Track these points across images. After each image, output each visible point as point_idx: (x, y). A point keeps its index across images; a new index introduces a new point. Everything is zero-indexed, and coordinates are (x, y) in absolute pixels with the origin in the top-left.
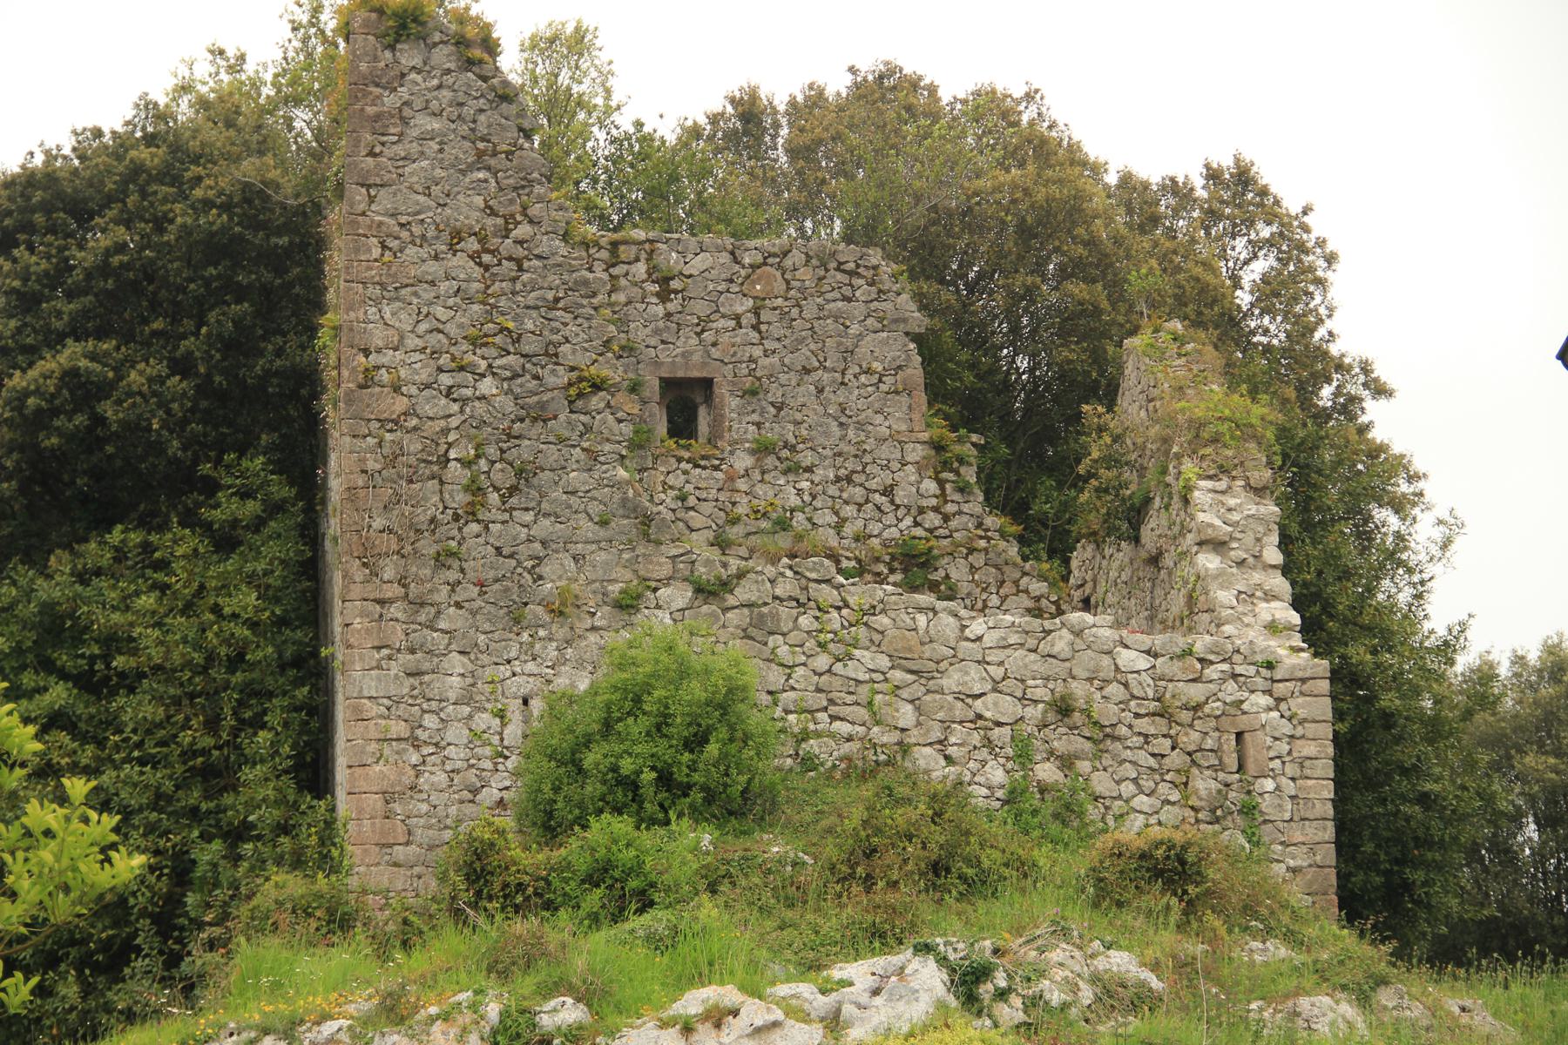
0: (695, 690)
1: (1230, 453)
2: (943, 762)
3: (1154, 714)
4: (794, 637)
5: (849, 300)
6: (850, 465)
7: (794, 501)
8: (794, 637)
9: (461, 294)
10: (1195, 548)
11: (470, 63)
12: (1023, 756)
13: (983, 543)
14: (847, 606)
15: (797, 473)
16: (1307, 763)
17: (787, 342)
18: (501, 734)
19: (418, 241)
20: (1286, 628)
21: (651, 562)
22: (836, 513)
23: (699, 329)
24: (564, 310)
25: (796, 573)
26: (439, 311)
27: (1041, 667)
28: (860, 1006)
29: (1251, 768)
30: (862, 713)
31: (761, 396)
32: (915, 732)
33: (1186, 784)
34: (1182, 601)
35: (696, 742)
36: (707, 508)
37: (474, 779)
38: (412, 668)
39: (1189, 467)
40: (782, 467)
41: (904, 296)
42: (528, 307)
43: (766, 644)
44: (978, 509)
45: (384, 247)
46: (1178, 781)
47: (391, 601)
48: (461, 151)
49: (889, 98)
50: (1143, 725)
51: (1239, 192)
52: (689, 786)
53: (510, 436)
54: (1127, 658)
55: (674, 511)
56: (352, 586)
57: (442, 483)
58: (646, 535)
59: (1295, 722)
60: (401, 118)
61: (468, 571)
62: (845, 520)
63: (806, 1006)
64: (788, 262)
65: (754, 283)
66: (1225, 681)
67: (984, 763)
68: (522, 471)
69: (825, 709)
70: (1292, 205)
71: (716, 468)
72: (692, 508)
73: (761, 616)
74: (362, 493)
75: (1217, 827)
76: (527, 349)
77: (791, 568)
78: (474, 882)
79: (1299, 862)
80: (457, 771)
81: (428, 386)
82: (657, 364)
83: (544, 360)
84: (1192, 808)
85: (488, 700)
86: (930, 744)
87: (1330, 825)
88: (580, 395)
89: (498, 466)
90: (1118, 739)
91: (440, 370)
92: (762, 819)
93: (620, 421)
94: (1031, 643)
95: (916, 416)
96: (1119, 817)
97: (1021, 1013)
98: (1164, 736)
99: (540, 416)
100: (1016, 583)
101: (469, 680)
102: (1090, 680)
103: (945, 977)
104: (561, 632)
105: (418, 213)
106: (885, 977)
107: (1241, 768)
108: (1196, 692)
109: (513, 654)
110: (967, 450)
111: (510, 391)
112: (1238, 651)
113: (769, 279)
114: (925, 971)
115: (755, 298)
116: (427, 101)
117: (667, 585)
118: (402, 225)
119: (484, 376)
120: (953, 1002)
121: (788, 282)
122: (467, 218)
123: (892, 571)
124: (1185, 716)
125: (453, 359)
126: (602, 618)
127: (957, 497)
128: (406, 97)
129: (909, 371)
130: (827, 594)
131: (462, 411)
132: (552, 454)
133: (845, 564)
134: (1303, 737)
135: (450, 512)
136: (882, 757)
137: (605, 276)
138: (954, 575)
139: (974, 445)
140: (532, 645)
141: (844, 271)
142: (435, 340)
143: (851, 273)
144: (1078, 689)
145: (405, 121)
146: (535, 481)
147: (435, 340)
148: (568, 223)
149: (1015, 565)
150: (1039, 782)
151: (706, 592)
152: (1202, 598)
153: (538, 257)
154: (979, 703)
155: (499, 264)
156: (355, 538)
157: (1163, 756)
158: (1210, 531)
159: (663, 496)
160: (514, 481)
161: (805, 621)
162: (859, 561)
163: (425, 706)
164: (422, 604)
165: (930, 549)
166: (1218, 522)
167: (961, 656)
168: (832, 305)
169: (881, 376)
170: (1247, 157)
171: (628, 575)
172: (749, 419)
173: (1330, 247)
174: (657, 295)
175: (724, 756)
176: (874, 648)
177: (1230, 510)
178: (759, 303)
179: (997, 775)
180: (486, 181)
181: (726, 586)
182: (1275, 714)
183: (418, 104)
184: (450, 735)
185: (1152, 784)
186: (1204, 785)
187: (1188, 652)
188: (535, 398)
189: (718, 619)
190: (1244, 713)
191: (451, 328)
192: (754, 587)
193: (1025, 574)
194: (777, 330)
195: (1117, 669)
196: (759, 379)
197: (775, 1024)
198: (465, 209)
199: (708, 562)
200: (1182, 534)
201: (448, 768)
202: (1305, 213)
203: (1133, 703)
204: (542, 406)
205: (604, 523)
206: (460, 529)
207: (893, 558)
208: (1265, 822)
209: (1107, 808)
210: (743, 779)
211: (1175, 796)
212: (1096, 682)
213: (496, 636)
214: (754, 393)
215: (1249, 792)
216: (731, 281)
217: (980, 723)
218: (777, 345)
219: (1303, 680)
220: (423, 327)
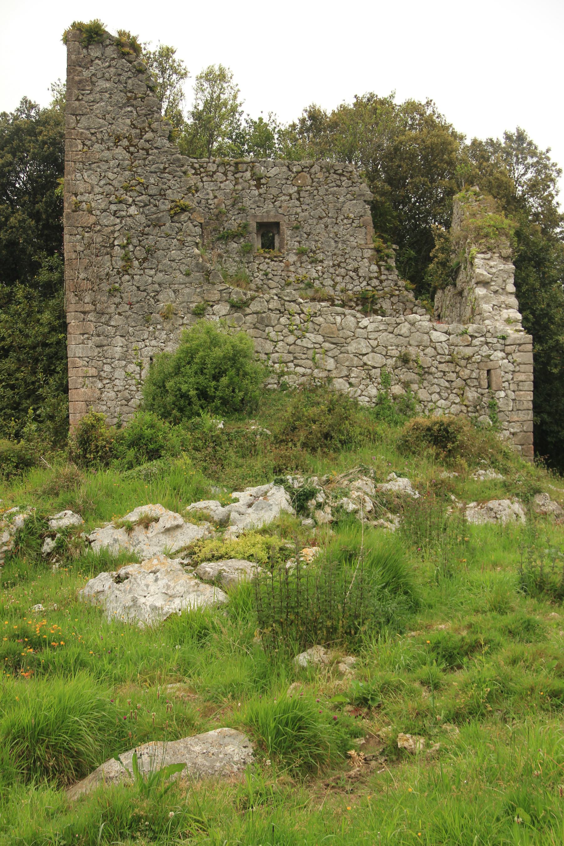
0: (218, 352)
1: (493, 241)
2: (348, 386)
3: (448, 362)
4: (278, 328)
5: (339, 186)
6: (339, 259)
7: (315, 275)
8: (278, 328)
9: (120, 166)
10: (475, 286)
11: (124, 55)
12: (386, 382)
13: (397, 292)
14: (303, 313)
15: (316, 263)
16: (521, 384)
17: (312, 206)
18: (140, 374)
19: (100, 141)
20: (515, 321)
21: (210, 293)
22: (333, 280)
23: (273, 201)
24: (169, 173)
25: (279, 297)
26: (110, 175)
27: (394, 340)
28: (240, 514)
29: (494, 386)
30: (310, 363)
32: (335, 372)
33: (463, 394)
34: (470, 310)
35: (216, 378)
36: (277, 279)
37: (127, 395)
38: (98, 343)
39: (474, 249)
40: (309, 260)
41: (364, 184)
42: (151, 172)
43: (264, 331)
44: (395, 278)
45: (84, 144)
46: (459, 393)
47: (88, 312)
48: (119, 97)
49: (372, 110)
50: (443, 367)
51: (519, 143)
52: (215, 397)
53: (143, 234)
54: (436, 335)
55: (262, 280)
56: (70, 305)
57: (112, 257)
58: (208, 280)
59: (515, 364)
60: (92, 82)
61: (124, 298)
62: (337, 283)
63: (212, 513)
64: (313, 170)
65: (297, 180)
66: (482, 345)
67: (367, 386)
68: (149, 250)
70: (542, 148)
71: (281, 261)
72: (270, 279)
73: (262, 318)
74: (74, 262)
75: (477, 414)
76: (151, 192)
77: (276, 295)
78: (84, 445)
79: (516, 430)
80: (120, 391)
81: (105, 211)
82: (255, 216)
83: (159, 197)
84: (466, 405)
85: (134, 358)
86: (342, 377)
87: (531, 412)
88: (175, 214)
89: (138, 248)
90: (431, 374)
91: (110, 203)
92: (251, 413)
93: (195, 226)
94: (390, 329)
95: (368, 237)
96: (431, 410)
97: (330, 516)
98: (453, 372)
99: (157, 224)
100: (411, 309)
101: (125, 349)
102: (418, 346)
103: (288, 497)
104: (168, 327)
105: (100, 128)
106: (256, 498)
107: (489, 387)
108: (468, 351)
109: (146, 337)
110: (391, 252)
111: (143, 213)
112: (489, 332)
113: (304, 178)
114: (279, 493)
115: (298, 186)
116: (104, 74)
117: (218, 304)
118: (92, 134)
119: (130, 205)
120: (291, 510)
121: (312, 179)
122: (123, 130)
123: (357, 305)
124: (463, 363)
125: (116, 197)
126: (187, 319)
127: (386, 272)
128: (94, 71)
129: (366, 218)
130: (294, 307)
131: (121, 222)
132: (163, 242)
133: (337, 302)
134: (519, 371)
135: (115, 270)
136: (319, 384)
137: (233, 178)
138: (384, 307)
139: (394, 250)
140: (154, 333)
141: (337, 174)
142: (108, 188)
143: (341, 175)
144: (412, 350)
145: (93, 83)
146: (155, 255)
147: (108, 188)
148: (170, 132)
149: (411, 302)
150: (393, 394)
151: (236, 307)
152: (477, 309)
154: (365, 358)
155: (138, 152)
156: (72, 283)
157: (452, 381)
158: (481, 277)
159: (258, 274)
160: (145, 255)
161: (283, 320)
162: (343, 301)
163: (104, 361)
164: (103, 314)
165: (374, 296)
166: (485, 273)
167: (357, 336)
168: (332, 189)
169: (353, 220)
170: (522, 128)
171: (200, 299)
172: (295, 240)
173: (558, 167)
174: (255, 186)
175: (231, 383)
176: (315, 333)
177: (491, 267)
178: (300, 188)
179: (373, 391)
180: (131, 112)
181: (246, 304)
182: (506, 361)
183: (99, 75)
184: (116, 375)
185: (447, 395)
188: (155, 216)
189: (242, 320)
190: (491, 361)
191: (115, 183)
192: (259, 304)
193: (415, 305)
195: (431, 341)
196: (300, 222)
197: (178, 527)
198: (122, 126)
199: (237, 293)
200: (470, 280)
201: (115, 390)
202: (547, 152)
203: (438, 357)
204: (158, 219)
205: (188, 275)
206: (120, 278)
207: (358, 299)
208: (500, 411)
209: (425, 406)
210: (241, 394)
211: (458, 400)
212: (421, 347)
213: (137, 328)
214: (297, 228)
215: (493, 398)
216: (288, 179)
217: (366, 367)
218: (307, 207)
219: (520, 345)
220: (102, 182)
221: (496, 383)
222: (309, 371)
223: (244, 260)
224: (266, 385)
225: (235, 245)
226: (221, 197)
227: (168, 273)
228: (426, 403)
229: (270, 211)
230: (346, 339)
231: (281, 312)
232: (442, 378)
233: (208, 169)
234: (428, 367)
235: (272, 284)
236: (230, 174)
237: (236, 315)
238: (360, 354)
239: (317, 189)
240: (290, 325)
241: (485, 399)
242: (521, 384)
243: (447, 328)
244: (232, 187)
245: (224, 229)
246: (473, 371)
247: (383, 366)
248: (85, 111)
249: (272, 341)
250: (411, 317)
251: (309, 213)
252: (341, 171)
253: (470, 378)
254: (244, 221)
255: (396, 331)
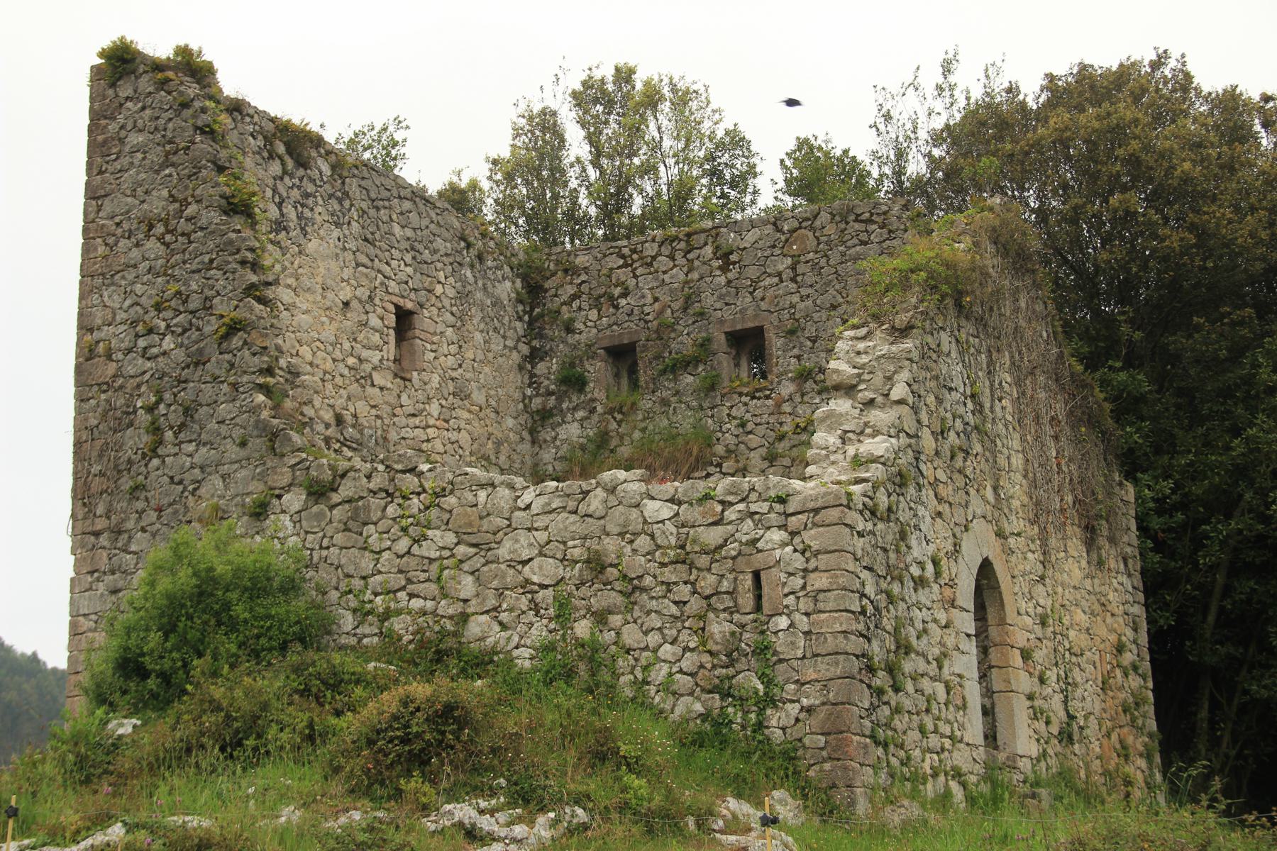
2: (497, 628)
3: (677, 562)
4: (383, 525)
5: (865, 243)
8: (383, 525)
12: (564, 615)
14: (424, 491)
15: (829, 392)
16: (821, 596)
17: (817, 287)
24: (217, 268)
26: (139, 288)
30: (433, 588)
31: (799, 334)
33: (703, 629)
36: (761, 430)
42: (193, 272)
43: (361, 534)
50: (669, 575)
53: (180, 382)
59: (808, 554)
60: (120, 139)
64: (818, 223)
69: (403, 588)
71: (768, 397)
72: (750, 432)
73: (357, 509)
75: (731, 671)
79: (812, 701)
81: (130, 351)
84: (710, 652)
86: (487, 612)
89: (173, 408)
91: (137, 336)
94: (572, 505)
98: (686, 583)
102: (622, 535)
105: (128, 212)
107: (758, 608)
108: (713, 536)
113: (803, 239)
115: (792, 257)
117: (288, 492)
119: (164, 335)
121: (817, 238)
124: (703, 561)
134: (816, 569)
137: (684, 261)
141: (862, 221)
144: (610, 545)
153: (202, 229)
158: (835, 377)
167: (514, 525)
171: (261, 487)
172: (792, 354)
174: (720, 268)
177: (859, 353)
186: (719, 628)
187: (707, 497)
190: (759, 551)
191: (144, 300)
194: (809, 279)
195: (645, 522)
196: (797, 320)
205: (243, 444)
208: (781, 661)
209: (636, 660)
214: (792, 332)
215: (763, 632)
216: (774, 246)
218: (810, 291)
219: (816, 511)
221: (770, 598)
222: (430, 605)
223: (706, 405)
224: (360, 640)
225: (690, 379)
226: (665, 298)
227: (215, 446)
228: (636, 654)
229: (745, 309)
230: (495, 534)
231: (389, 495)
232: (665, 597)
233: (645, 253)
234: (638, 577)
235: (753, 440)
236: (678, 255)
237: (315, 509)
238: (520, 562)
239: (826, 256)
240: (402, 517)
241: (746, 636)
242: (821, 596)
243: (672, 491)
244: (682, 277)
245: (670, 353)
246: (723, 576)
247: (557, 584)
248: (108, 187)
249: (372, 551)
250: (607, 476)
251: (814, 302)
252: (867, 215)
253: (718, 593)
254: (704, 334)
255: (582, 509)
